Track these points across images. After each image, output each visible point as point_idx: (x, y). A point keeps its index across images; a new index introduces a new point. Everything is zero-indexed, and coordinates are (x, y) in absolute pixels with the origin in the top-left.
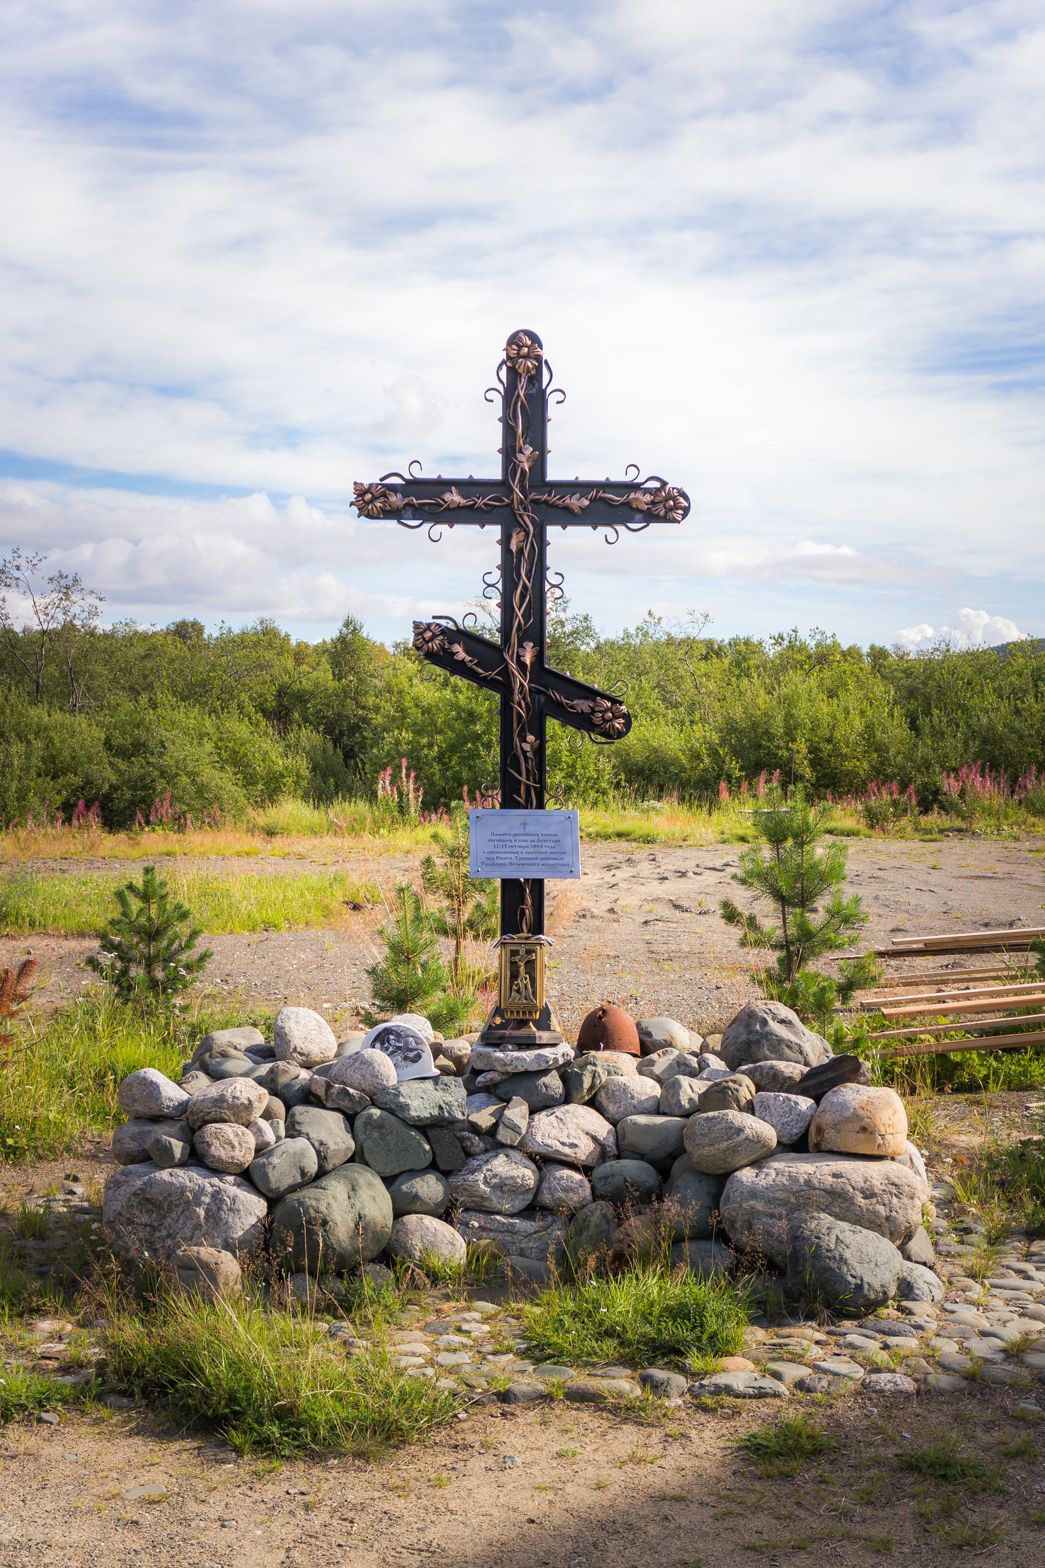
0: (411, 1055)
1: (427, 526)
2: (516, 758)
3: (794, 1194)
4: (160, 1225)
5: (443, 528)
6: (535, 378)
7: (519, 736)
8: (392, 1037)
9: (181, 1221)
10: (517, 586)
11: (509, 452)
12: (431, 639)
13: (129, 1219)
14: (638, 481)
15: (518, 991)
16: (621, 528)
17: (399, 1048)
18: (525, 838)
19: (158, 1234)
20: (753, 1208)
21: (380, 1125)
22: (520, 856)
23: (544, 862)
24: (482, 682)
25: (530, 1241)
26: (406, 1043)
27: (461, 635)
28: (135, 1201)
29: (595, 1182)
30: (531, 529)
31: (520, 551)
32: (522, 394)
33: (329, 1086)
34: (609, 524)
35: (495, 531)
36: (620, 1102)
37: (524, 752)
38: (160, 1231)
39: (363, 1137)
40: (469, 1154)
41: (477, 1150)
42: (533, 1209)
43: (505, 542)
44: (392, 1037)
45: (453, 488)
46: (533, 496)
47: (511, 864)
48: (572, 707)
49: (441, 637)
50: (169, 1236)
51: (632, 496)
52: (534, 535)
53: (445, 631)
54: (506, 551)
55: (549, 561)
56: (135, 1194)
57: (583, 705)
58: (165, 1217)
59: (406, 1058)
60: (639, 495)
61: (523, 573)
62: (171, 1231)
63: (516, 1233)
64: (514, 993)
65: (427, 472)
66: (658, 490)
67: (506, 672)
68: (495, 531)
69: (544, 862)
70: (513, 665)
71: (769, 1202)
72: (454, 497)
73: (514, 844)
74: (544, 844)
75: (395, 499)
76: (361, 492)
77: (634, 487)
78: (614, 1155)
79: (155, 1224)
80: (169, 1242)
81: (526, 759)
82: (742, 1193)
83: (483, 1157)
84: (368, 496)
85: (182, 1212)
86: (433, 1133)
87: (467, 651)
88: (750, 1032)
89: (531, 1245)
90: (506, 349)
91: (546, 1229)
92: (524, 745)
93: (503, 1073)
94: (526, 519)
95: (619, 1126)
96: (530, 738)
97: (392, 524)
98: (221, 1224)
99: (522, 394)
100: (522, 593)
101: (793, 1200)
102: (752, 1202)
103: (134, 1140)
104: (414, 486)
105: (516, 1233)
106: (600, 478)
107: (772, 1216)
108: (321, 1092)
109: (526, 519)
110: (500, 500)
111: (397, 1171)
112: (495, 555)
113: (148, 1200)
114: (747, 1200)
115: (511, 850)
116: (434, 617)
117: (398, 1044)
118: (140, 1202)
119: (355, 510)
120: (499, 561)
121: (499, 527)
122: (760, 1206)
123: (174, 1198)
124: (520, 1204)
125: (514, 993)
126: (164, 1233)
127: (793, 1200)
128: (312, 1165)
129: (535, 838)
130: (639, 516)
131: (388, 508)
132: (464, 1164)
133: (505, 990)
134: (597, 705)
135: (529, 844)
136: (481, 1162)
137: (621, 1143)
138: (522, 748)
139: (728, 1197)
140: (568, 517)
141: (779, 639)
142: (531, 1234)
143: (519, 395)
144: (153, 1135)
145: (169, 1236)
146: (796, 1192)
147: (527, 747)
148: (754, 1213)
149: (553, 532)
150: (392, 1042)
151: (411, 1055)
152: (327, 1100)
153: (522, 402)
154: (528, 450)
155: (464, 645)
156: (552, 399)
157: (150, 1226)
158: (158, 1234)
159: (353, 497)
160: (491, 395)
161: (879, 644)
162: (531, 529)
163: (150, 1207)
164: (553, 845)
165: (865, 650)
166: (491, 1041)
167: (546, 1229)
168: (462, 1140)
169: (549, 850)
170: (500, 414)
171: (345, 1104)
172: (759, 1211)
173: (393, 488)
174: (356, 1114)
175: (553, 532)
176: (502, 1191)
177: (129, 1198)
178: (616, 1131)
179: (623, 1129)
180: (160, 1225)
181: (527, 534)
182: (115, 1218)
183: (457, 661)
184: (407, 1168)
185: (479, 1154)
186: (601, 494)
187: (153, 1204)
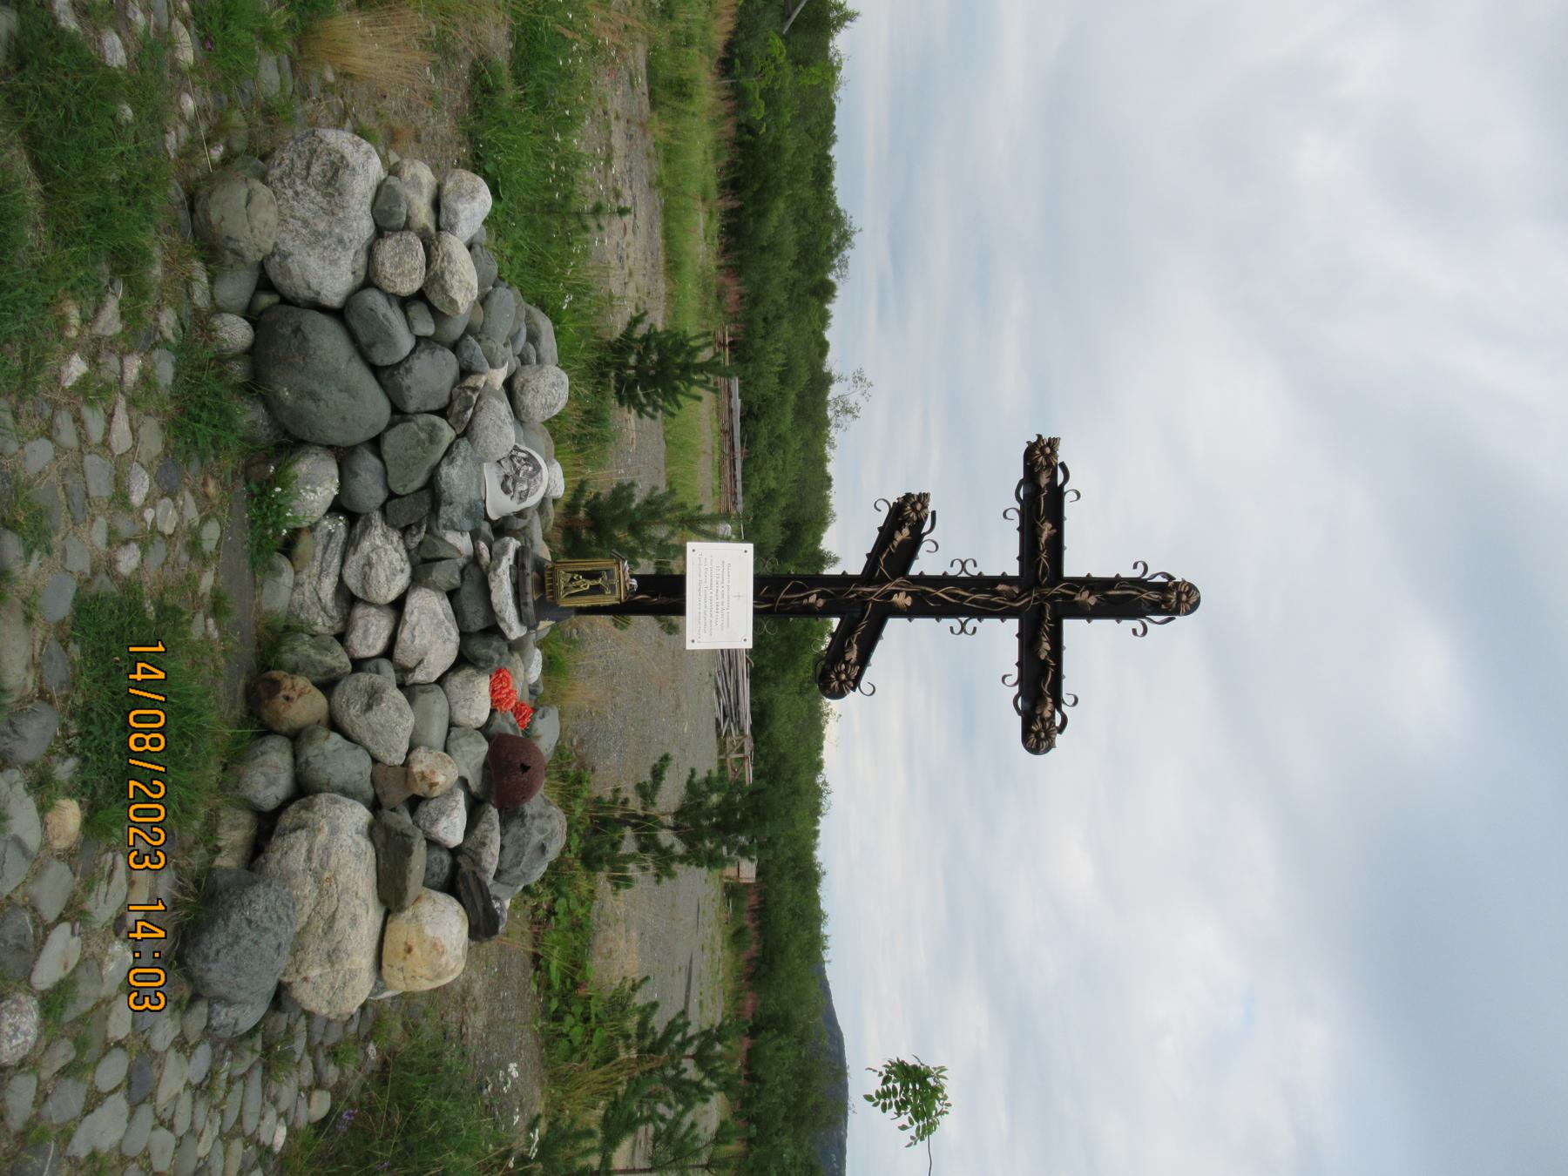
0: (509, 483)
1: (1018, 506)
2: (802, 589)
3: (334, 876)
4: (308, 184)
5: (1017, 523)
6: (1156, 608)
7: (823, 592)
8: (530, 469)
9: (312, 206)
10: (965, 590)
11: (1089, 583)
12: (914, 509)
13: (316, 151)
14: (1063, 707)
15: (572, 580)
16: (1016, 690)
17: (518, 472)
18: (725, 596)
19: (298, 182)
20: (319, 830)
21: (433, 439)
22: (708, 592)
23: (702, 615)
24: (873, 558)
25: (312, 593)
26: (522, 481)
27: (916, 540)
28: (335, 157)
29: (374, 662)
30: (1018, 604)
31: (998, 594)
32: (1144, 596)
33: (474, 389)
34: (1020, 681)
35: (1013, 570)
36: (462, 688)
37: (807, 597)
38: (302, 184)
39: (420, 423)
40: (405, 531)
41: (408, 541)
42: (348, 600)
43: (1004, 579)
44: (530, 469)
45: (1054, 531)
46: (1048, 606)
47: (701, 581)
48: (850, 644)
49: (915, 518)
50: (297, 193)
51: (1050, 700)
52: (1011, 607)
53: (921, 523)
54: (994, 581)
55: (987, 622)
56: (343, 157)
57: (852, 655)
58: (317, 189)
59: (506, 477)
60: (1050, 706)
61: (977, 596)
62: (301, 196)
63: (319, 578)
64: (570, 576)
65: (1070, 507)
66: (1052, 723)
67: (883, 581)
68: (1013, 570)
69: (702, 615)
70: (889, 587)
71: (326, 849)
72: (1047, 529)
73: (720, 586)
74: (720, 614)
75: (1044, 480)
76: (1053, 443)
77: (1058, 703)
78: (404, 682)
79: (310, 180)
80: (290, 193)
81: (801, 599)
82: (338, 818)
83: (401, 547)
84: (1048, 450)
85: (322, 208)
86: (426, 496)
87: (902, 543)
88: (533, 818)
89: (307, 594)
90: (1184, 582)
91: (324, 609)
92: (815, 596)
93: (487, 567)
94: (1027, 600)
95: (435, 686)
96: (821, 602)
97: (1019, 474)
98: (308, 249)
99: (1144, 596)
100: (958, 594)
101: (327, 875)
102: (326, 829)
103: (412, 178)
104: (1057, 494)
105: (319, 578)
106: (1065, 671)
107: (310, 851)
108: (470, 382)
109: (1027, 600)
110: (1044, 574)
111: (386, 457)
112: (991, 570)
113: (337, 171)
114: (329, 823)
115: (714, 583)
116: (934, 513)
117: (522, 472)
118: (334, 163)
119: (1034, 439)
120: (986, 573)
121: (1017, 573)
122: (322, 838)
123: (337, 199)
124: (353, 582)
125: (570, 576)
126: (300, 188)
127: (327, 875)
128: (382, 357)
129: (725, 606)
130: (1028, 706)
131: (1036, 470)
132: (393, 526)
133: (573, 567)
134: (854, 666)
135: (720, 601)
136: (395, 544)
137: (418, 688)
138: (812, 594)
139: (336, 802)
140: (1028, 642)
141: (825, 783)
142: (317, 594)
143: (1143, 593)
144: (417, 197)
145: (297, 193)
146: (336, 879)
147: (812, 599)
148: (315, 831)
149: (1013, 625)
150: (525, 468)
151: (509, 483)
152: (460, 388)
153: (1136, 596)
154: (1092, 601)
155: (909, 541)
156: (1136, 624)
157: (308, 174)
158: (298, 182)
159: (1046, 437)
160: (1141, 568)
161: (821, 834)
162: (1018, 604)
163: (329, 174)
164: (719, 624)
165: (818, 828)
166: (520, 555)
167: (324, 609)
168: (419, 526)
169: (720, 601)
170: (1123, 575)
171: (457, 407)
172: (315, 836)
173: (1054, 476)
174: (447, 418)
175: (1013, 625)
176: (364, 565)
177: (338, 152)
178: (430, 684)
179: (432, 691)
180: (308, 184)
181: (1013, 600)
182: (317, 136)
183: (894, 533)
184: (389, 467)
185: (405, 543)
186: (1051, 670)
187: (332, 177)
